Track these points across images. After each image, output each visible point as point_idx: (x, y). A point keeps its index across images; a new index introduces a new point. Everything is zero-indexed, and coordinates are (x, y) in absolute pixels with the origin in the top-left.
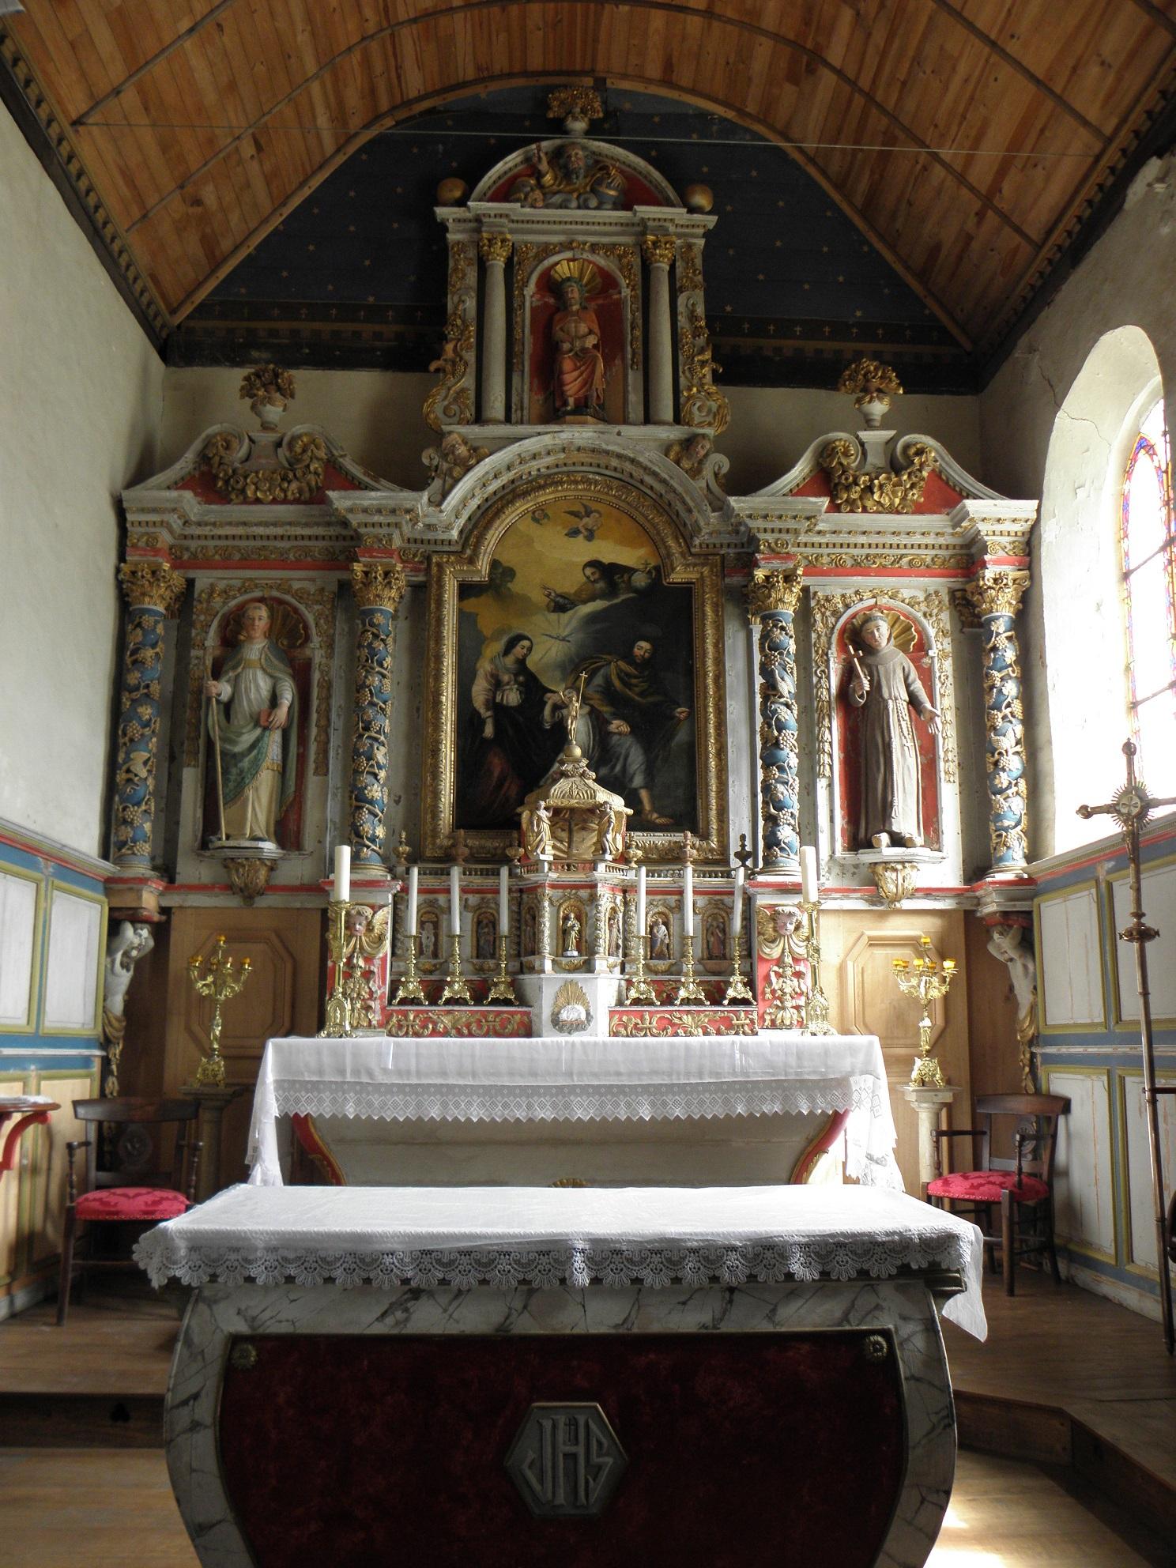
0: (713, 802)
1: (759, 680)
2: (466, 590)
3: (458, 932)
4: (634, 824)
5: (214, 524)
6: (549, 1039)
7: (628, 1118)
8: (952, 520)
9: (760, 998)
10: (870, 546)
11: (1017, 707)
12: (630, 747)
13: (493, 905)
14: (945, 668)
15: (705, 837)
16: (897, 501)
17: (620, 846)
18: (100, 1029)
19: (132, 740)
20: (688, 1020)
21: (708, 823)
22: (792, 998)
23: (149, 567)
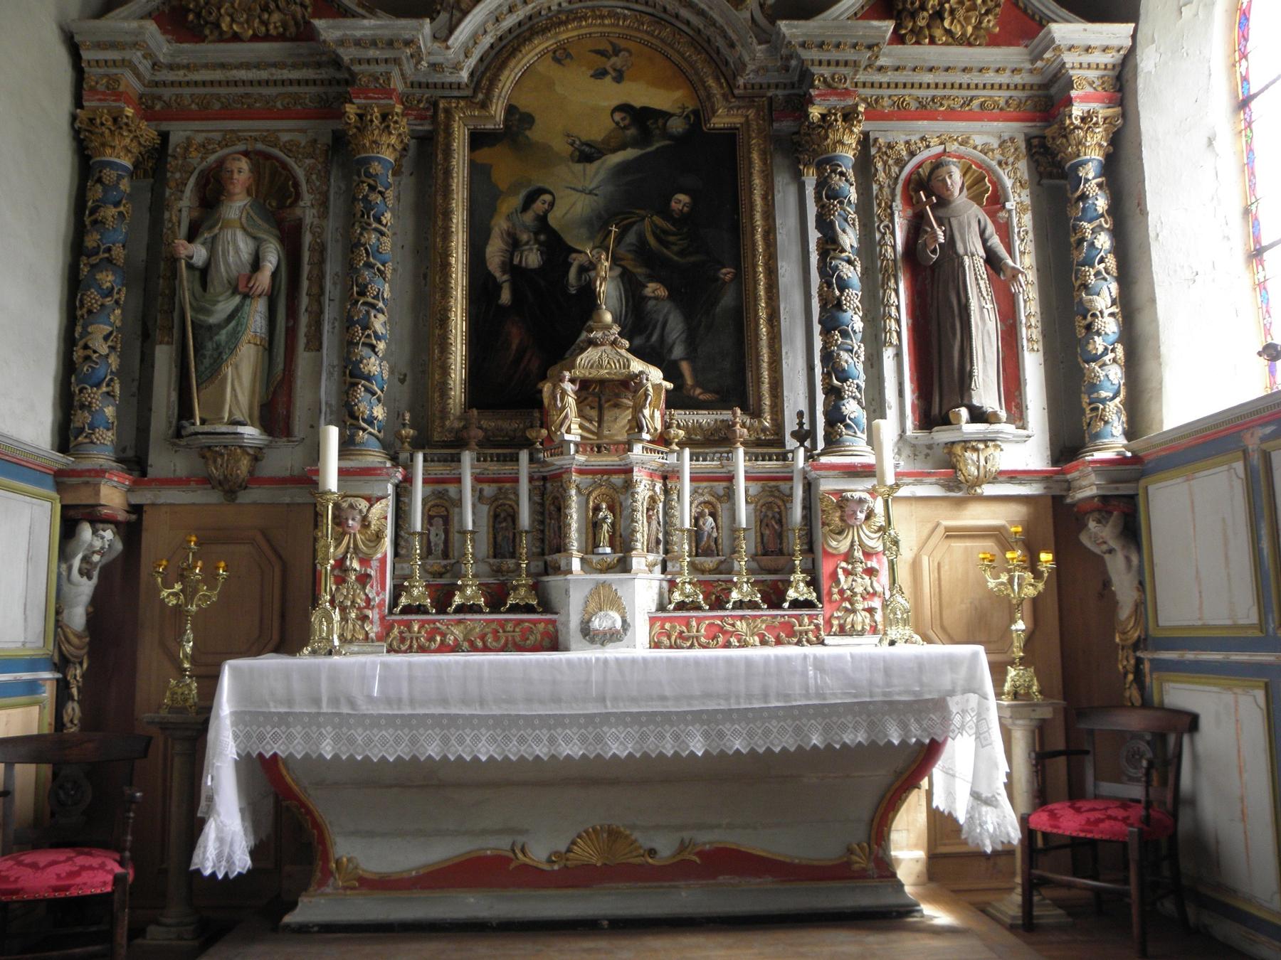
0: (766, 374)
1: (814, 235)
2: (478, 140)
3: (470, 527)
4: (675, 400)
5: (187, 67)
6: (580, 654)
7: (676, 752)
8: (1030, 54)
9: (825, 599)
10: (937, 86)
11: (1111, 262)
12: (668, 313)
13: (512, 496)
14: (1024, 222)
15: (757, 414)
16: (970, 29)
17: (659, 425)
18: (51, 646)
19: (90, 312)
20: (741, 626)
21: (760, 398)
22: (864, 599)
23: (109, 112)
